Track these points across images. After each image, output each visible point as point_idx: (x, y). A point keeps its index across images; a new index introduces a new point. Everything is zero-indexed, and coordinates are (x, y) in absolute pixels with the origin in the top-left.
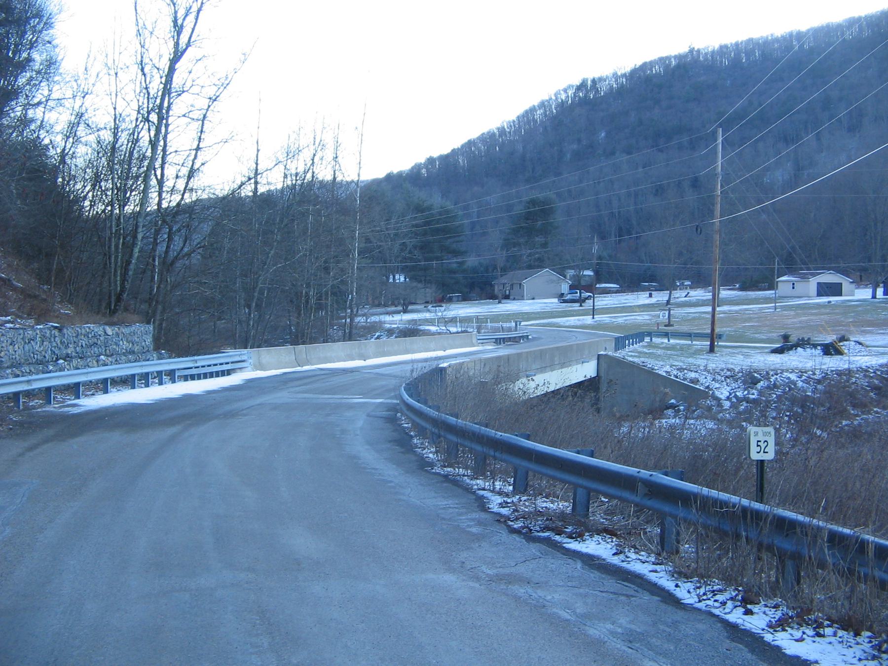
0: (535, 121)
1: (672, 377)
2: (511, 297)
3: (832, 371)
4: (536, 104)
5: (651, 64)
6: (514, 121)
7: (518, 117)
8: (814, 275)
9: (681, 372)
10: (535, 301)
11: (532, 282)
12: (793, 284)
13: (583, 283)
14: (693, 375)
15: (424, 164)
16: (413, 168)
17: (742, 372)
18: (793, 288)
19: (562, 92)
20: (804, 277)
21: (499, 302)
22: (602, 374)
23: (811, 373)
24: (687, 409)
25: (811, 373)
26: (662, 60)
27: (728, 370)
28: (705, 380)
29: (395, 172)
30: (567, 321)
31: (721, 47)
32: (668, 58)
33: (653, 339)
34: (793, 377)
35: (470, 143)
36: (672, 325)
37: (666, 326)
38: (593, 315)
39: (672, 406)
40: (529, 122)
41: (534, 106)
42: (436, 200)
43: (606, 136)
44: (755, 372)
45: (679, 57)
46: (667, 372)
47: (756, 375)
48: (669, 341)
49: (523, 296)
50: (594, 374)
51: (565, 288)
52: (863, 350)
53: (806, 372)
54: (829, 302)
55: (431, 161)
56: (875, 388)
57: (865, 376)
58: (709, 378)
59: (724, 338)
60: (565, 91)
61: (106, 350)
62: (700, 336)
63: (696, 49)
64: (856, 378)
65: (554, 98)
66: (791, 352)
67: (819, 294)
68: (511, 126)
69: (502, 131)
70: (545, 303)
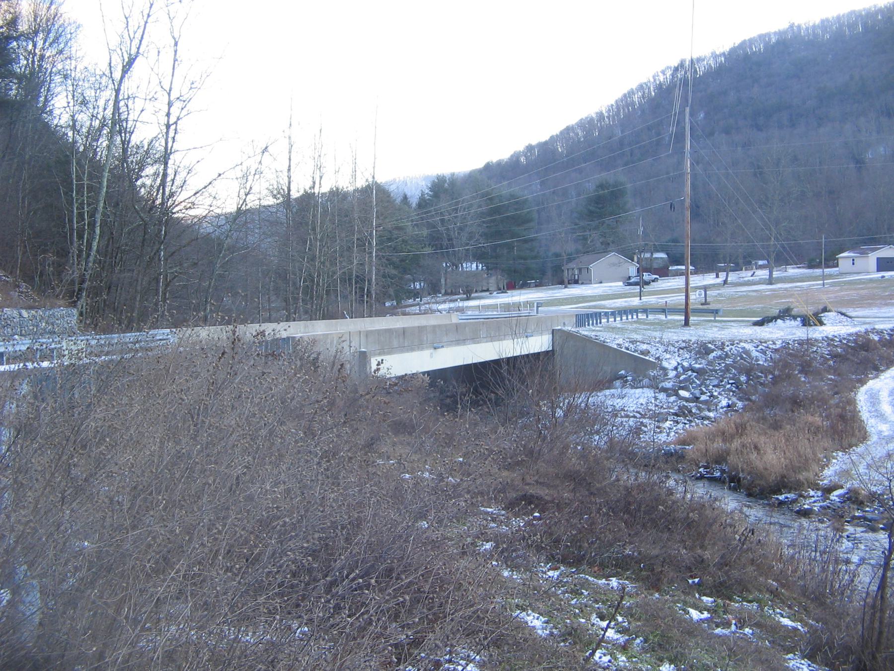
0: (633, 103)
1: (623, 350)
2: (580, 282)
3: (794, 341)
4: (634, 88)
5: (751, 41)
6: (612, 105)
7: (616, 101)
8: (874, 250)
9: (633, 344)
10: (602, 285)
11: (597, 267)
12: (853, 260)
13: (655, 266)
14: (644, 347)
15: (523, 152)
16: (512, 156)
17: (697, 343)
18: (853, 264)
19: (660, 74)
20: (864, 253)
21: (566, 287)
22: (557, 348)
23: (771, 342)
24: (634, 380)
25: (771, 342)
26: (761, 37)
27: (683, 341)
28: (656, 351)
29: (494, 161)
30: (615, 303)
31: (822, 21)
32: (768, 35)
33: (639, 315)
34: (748, 346)
35: (568, 129)
36: (709, 304)
37: (702, 304)
38: (640, 297)
39: (622, 377)
40: (628, 106)
41: (632, 89)
42: (505, 189)
43: (705, 118)
44: (710, 343)
45: (780, 33)
46: (618, 344)
47: (710, 345)
48: (647, 317)
49: (590, 281)
50: (551, 349)
51: (632, 270)
52: (844, 320)
53: (765, 342)
54: (883, 277)
55: (530, 148)
56: (834, 356)
57: (828, 345)
58: (662, 348)
59: (720, 313)
60: (663, 72)
61: (21, 331)
62: (674, 311)
63: (796, 24)
64: (818, 347)
65: (652, 80)
66: (770, 324)
67: (879, 269)
68: (609, 110)
69: (600, 115)
70: (610, 287)
